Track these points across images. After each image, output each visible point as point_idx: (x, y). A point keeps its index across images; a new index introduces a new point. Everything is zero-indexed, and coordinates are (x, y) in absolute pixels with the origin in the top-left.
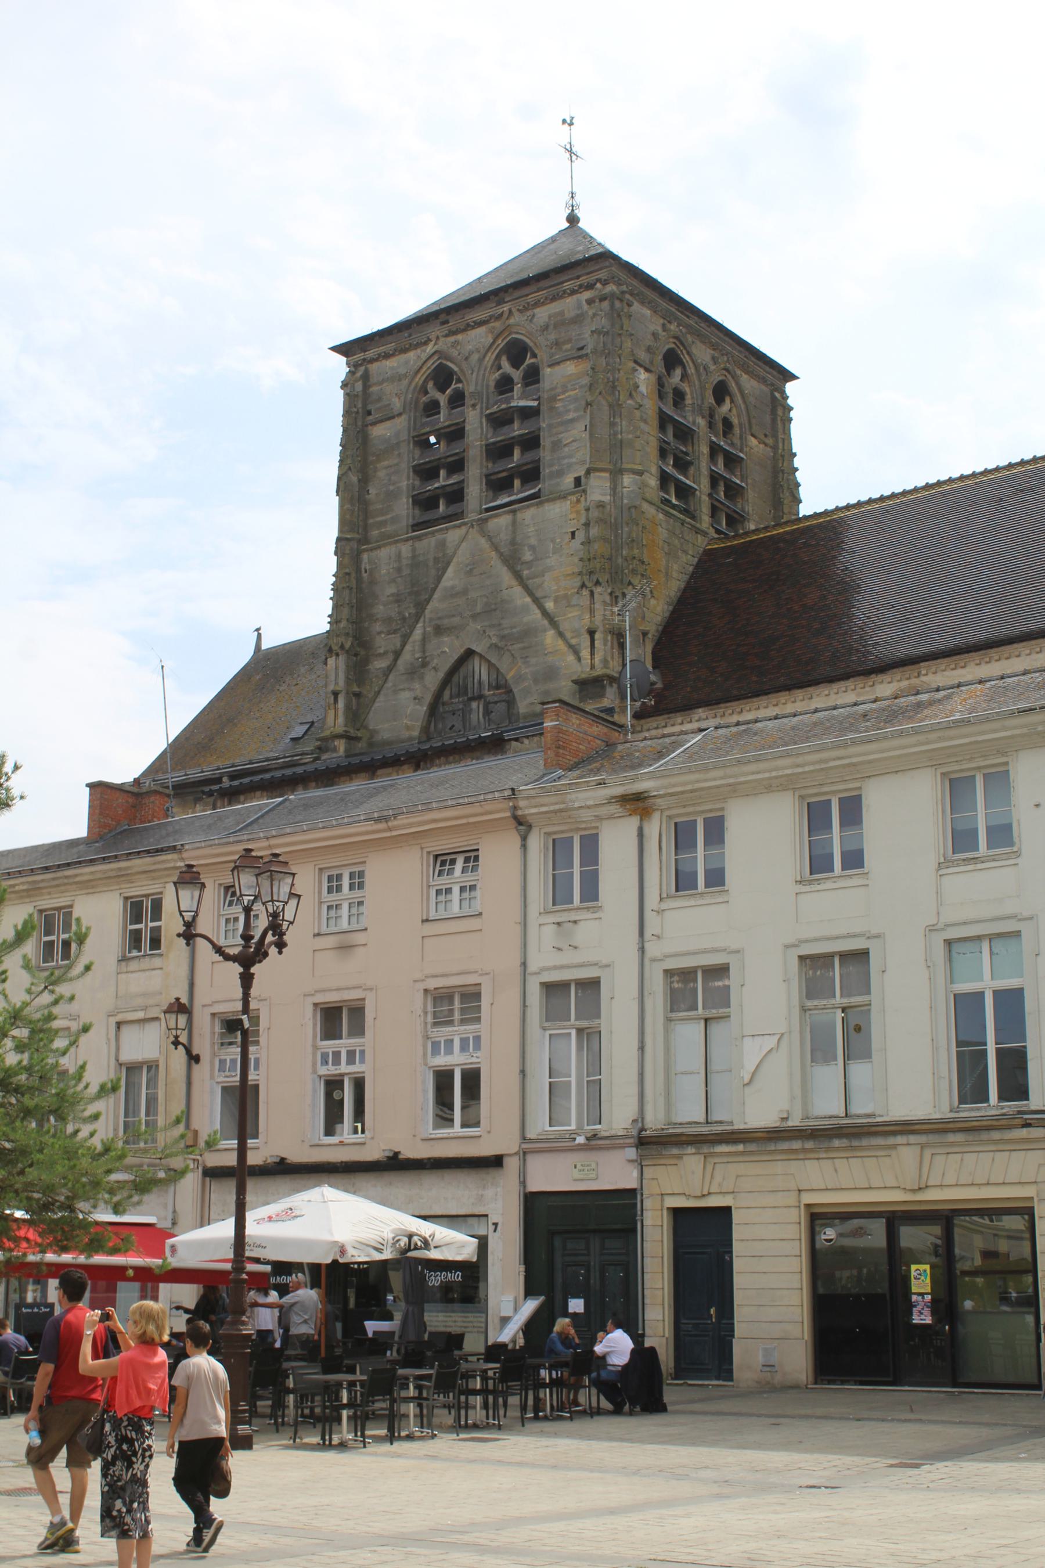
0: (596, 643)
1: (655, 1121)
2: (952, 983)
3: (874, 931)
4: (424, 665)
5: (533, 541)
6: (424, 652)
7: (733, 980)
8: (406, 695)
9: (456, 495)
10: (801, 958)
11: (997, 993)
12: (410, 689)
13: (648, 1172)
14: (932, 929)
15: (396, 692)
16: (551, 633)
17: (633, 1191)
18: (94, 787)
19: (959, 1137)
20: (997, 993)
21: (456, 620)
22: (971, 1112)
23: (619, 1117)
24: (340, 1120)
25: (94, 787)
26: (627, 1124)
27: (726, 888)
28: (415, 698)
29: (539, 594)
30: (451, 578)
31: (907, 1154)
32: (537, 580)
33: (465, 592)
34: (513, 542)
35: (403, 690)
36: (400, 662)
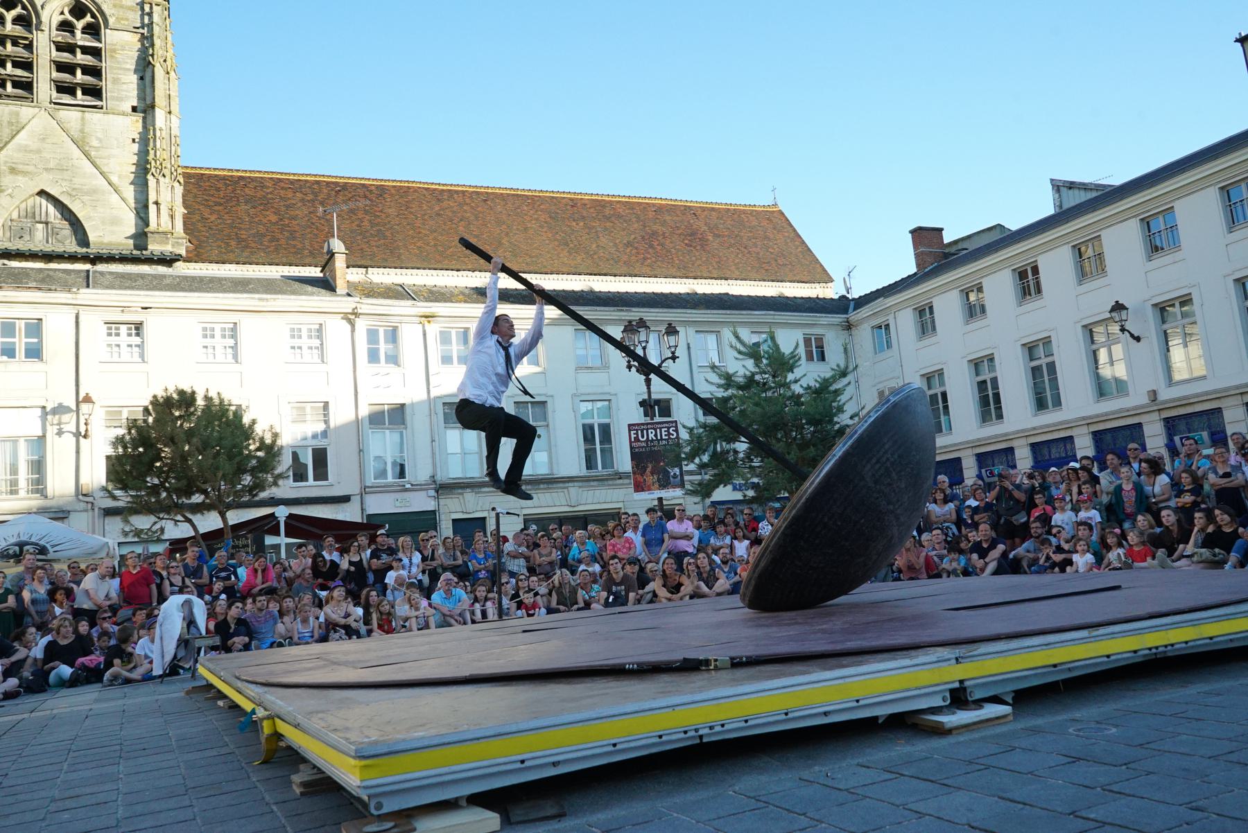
1: (442, 477)
2: (1164, 322)
3: (842, 349)
5: (99, 135)
7: (1196, 306)
9: (27, 86)
11: (599, 425)
13: (442, 502)
14: (574, 395)
17: (434, 512)
18: (912, 232)
19: (595, 483)
20: (599, 425)
21: (30, 168)
22: (593, 473)
23: (420, 472)
25: (912, 232)
26: (427, 478)
29: (105, 169)
30: (22, 138)
31: (574, 490)
32: (105, 161)
33: (39, 151)
34: (82, 131)
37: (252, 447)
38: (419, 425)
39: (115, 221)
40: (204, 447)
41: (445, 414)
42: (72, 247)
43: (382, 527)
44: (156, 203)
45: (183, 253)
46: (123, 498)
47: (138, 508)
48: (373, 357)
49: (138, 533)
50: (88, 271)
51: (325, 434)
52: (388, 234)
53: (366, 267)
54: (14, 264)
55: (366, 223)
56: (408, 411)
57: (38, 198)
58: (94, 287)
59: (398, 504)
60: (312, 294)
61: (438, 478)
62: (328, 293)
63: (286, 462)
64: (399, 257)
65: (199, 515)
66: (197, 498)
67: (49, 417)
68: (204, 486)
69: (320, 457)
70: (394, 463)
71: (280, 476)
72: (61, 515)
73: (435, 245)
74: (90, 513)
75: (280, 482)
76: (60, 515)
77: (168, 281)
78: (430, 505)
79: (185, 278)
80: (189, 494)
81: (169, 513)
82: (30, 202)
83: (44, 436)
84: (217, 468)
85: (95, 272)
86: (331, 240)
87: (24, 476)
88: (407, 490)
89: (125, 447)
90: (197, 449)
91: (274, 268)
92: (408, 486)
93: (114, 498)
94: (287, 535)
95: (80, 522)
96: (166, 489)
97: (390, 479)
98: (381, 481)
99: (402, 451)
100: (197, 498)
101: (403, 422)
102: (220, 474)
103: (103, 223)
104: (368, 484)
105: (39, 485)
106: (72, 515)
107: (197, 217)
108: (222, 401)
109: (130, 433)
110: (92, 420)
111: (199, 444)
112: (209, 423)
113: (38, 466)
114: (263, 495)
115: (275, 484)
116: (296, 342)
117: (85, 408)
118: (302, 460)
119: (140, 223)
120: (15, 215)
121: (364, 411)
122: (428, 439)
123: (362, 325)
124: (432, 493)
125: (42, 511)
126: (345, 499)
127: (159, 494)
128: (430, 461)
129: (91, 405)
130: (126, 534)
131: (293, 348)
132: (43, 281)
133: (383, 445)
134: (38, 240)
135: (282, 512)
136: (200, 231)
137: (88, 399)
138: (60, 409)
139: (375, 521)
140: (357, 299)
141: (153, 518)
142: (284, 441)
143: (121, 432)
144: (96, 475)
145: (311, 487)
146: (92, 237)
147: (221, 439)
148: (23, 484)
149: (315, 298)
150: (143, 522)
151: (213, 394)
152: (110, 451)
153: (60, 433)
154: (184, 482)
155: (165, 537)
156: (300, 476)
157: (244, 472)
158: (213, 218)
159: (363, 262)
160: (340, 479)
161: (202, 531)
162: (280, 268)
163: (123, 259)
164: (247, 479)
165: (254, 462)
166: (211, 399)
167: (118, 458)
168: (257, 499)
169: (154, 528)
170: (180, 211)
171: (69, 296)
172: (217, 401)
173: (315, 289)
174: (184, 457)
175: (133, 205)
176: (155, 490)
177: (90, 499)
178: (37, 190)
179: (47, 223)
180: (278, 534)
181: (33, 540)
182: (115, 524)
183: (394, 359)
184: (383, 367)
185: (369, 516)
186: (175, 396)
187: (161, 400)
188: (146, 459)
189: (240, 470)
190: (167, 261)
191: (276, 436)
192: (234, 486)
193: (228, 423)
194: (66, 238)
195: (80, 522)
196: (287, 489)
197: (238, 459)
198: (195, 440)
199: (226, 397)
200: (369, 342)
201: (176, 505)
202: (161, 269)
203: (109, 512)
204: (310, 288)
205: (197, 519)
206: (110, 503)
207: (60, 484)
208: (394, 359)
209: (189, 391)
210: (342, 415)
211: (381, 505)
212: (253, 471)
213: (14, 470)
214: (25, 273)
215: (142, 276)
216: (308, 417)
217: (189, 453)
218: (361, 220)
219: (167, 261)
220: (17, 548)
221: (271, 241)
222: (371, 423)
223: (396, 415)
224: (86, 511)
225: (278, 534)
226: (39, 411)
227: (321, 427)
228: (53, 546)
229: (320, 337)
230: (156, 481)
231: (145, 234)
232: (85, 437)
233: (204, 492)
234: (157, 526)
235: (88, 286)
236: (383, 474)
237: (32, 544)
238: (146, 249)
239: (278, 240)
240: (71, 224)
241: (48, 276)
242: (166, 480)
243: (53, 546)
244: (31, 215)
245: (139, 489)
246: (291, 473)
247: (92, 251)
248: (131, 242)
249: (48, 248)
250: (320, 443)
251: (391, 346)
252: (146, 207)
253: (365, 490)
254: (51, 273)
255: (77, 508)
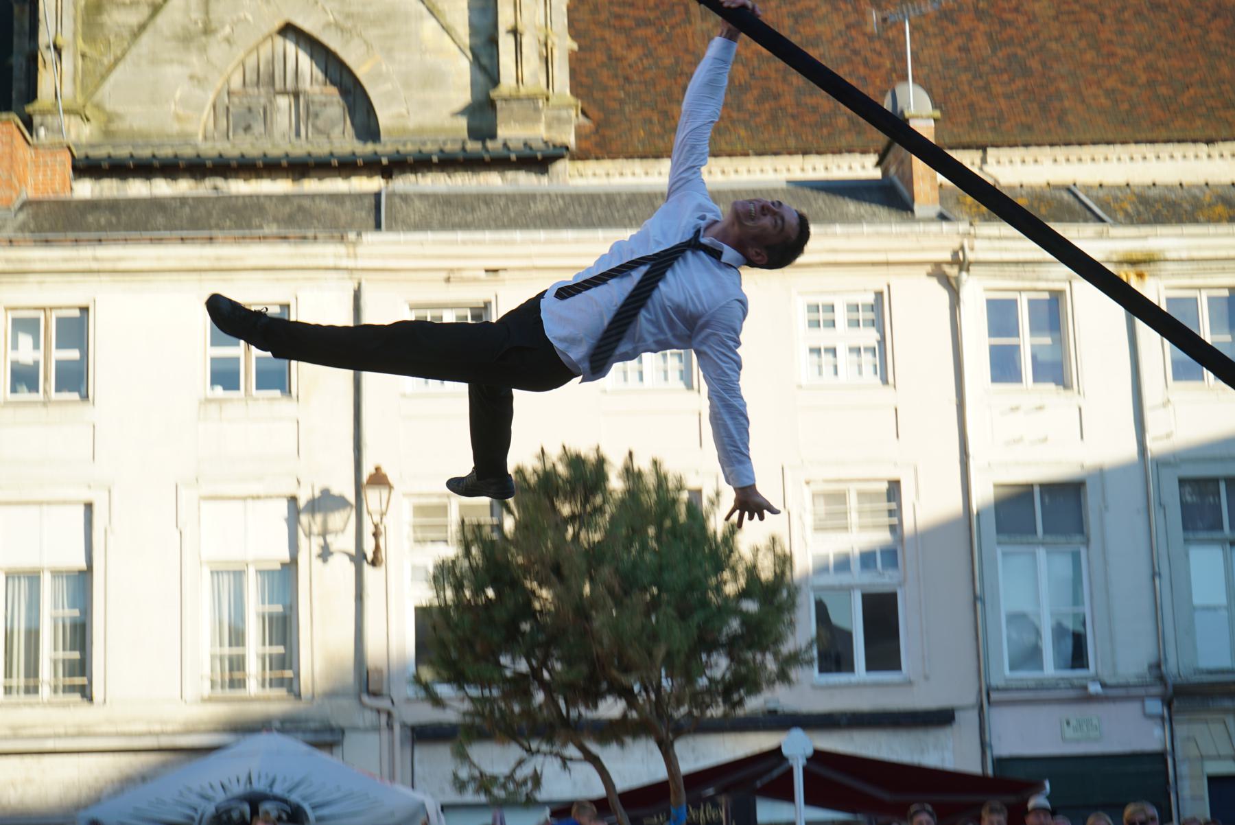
0: (525, 50)
4: (207, 31)
6: (207, 13)
8: (173, 72)
10: (1182, 482)
12: (181, 63)
13: (1181, 730)
15: (155, 61)
16: (430, 24)
17: (1159, 758)
23: (1124, 653)
24: (426, 516)
27: (10, 315)
28: (192, 77)
35: (171, 61)
36: (161, 19)
37: (730, 589)
38: (1119, 529)
39: (432, 79)
40: (629, 583)
41: (1184, 505)
42: (345, 142)
43: (1035, 787)
44: (515, 32)
45: (571, 140)
46: (455, 704)
47: (486, 727)
48: (1004, 366)
49: (485, 783)
50: (377, 196)
51: (890, 555)
52: (1034, 64)
53: (984, 148)
54: (239, 187)
55: (980, 42)
56: (1092, 499)
57: (279, 41)
58: (390, 228)
59: (1069, 733)
60: (858, 220)
61: (1171, 668)
62: (895, 215)
63: (802, 631)
64: (1061, 120)
65: (614, 748)
66: (611, 708)
67: (304, 519)
68: (624, 680)
69: (881, 613)
70: (1059, 631)
71: (795, 659)
72: (328, 737)
73: (1151, 84)
74: (385, 734)
75: (794, 673)
76: (327, 737)
77: (539, 207)
78: (1150, 738)
79: (577, 199)
80: (593, 698)
81: (550, 740)
82: (265, 51)
83: (294, 561)
84: (654, 637)
85: (391, 196)
86: (900, 89)
87: (255, 648)
88: (1090, 699)
89: (458, 588)
90: (611, 592)
91: (768, 162)
92: (1094, 688)
93: (437, 701)
94: (810, 800)
95: (366, 753)
96: (544, 685)
97: (1050, 669)
98: (1027, 675)
99: (1077, 599)
100: (611, 708)
101: (1079, 526)
102: (660, 652)
103: (407, 85)
104: (996, 681)
105: (284, 664)
106: (350, 740)
107: (600, 57)
108: (661, 480)
109: (468, 553)
110: (389, 523)
111: (615, 583)
112: (636, 532)
113: (283, 628)
114: (753, 704)
115: (783, 676)
116: (823, 337)
117: (373, 497)
118: (836, 618)
119: (481, 79)
120: (236, 82)
121: (983, 495)
122: (1145, 571)
123: (976, 291)
124: (1155, 707)
125: (288, 725)
126: (942, 718)
127: (527, 695)
128: (1149, 626)
129: (385, 493)
130: (460, 785)
131: (816, 351)
132: (290, 221)
133: (1031, 586)
134: (281, 135)
135: (798, 747)
136: (605, 89)
137: (379, 479)
138: (325, 502)
139: (1019, 774)
140: (963, 227)
141: (514, 752)
142: (803, 564)
143: (451, 551)
144: (395, 638)
145: (860, 688)
146: (385, 117)
147: (661, 568)
148: (253, 667)
149: (866, 229)
150: (496, 759)
151: (642, 464)
152: (426, 595)
153: (325, 554)
154: (584, 669)
155: (542, 795)
156: (834, 657)
157: (711, 646)
158: (633, 56)
159: (976, 137)
160: (931, 668)
161: (621, 785)
162: (782, 162)
163: (449, 163)
164: (720, 666)
165: (735, 624)
166: (639, 475)
167: (443, 610)
168: (740, 712)
169: (521, 774)
170: (564, 45)
171: (341, 249)
172: (650, 481)
173: (865, 208)
174: (582, 611)
175: (466, 40)
176: (519, 687)
177: (384, 704)
178: (278, 24)
179: (296, 95)
180: (789, 797)
181: (278, 790)
182: (438, 763)
183: (1055, 371)
184: (1029, 391)
185: (999, 762)
186: (562, 469)
187: (533, 480)
188: (501, 615)
189: (706, 643)
190: (537, 161)
191: (784, 561)
192: (690, 679)
193: (676, 532)
194: (333, 124)
195: (366, 753)
196: (810, 690)
197: (698, 617)
198: (606, 571)
199: (671, 468)
200: (994, 330)
201: (565, 722)
202: (524, 181)
203: (423, 735)
204: (851, 207)
205: (610, 755)
206: (426, 714)
207: (323, 649)
208: (1055, 371)
209: (592, 456)
210: (932, 502)
211: (1027, 734)
212: (733, 647)
213: (237, 637)
214: (256, 205)
215: (487, 199)
216: (853, 518)
217: (594, 601)
218: (969, 36)
219: (537, 161)
220: (246, 808)
221: (760, 100)
222: (1001, 529)
223: (1051, 510)
224: (376, 729)
225: (789, 797)
226: (283, 507)
227: (880, 537)
228: (314, 808)
229: (878, 323)
230: (523, 666)
231: (492, 104)
232: (374, 563)
233: (626, 693)
234: (525, 772)
235: (378, 226)
236: (1032, 656)
237: (275, 798)
238: (493, 136)
239: (776, 97)
240: (344, 93)
241: (300, 208)
242: (544, 664)
243: (314, 808)
244: (267, 79)
245: (484, 683)
246: (815, 653)
247: (385, 148)
248: (463, 123)
249: (300, 148)
250: (881, 581)
251: (1047, 340)
252: (493, 42)
253: (987, 698)
254: (307, 203)
255: (360, 723)
